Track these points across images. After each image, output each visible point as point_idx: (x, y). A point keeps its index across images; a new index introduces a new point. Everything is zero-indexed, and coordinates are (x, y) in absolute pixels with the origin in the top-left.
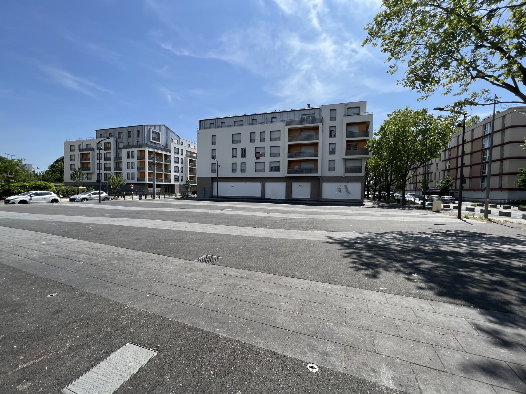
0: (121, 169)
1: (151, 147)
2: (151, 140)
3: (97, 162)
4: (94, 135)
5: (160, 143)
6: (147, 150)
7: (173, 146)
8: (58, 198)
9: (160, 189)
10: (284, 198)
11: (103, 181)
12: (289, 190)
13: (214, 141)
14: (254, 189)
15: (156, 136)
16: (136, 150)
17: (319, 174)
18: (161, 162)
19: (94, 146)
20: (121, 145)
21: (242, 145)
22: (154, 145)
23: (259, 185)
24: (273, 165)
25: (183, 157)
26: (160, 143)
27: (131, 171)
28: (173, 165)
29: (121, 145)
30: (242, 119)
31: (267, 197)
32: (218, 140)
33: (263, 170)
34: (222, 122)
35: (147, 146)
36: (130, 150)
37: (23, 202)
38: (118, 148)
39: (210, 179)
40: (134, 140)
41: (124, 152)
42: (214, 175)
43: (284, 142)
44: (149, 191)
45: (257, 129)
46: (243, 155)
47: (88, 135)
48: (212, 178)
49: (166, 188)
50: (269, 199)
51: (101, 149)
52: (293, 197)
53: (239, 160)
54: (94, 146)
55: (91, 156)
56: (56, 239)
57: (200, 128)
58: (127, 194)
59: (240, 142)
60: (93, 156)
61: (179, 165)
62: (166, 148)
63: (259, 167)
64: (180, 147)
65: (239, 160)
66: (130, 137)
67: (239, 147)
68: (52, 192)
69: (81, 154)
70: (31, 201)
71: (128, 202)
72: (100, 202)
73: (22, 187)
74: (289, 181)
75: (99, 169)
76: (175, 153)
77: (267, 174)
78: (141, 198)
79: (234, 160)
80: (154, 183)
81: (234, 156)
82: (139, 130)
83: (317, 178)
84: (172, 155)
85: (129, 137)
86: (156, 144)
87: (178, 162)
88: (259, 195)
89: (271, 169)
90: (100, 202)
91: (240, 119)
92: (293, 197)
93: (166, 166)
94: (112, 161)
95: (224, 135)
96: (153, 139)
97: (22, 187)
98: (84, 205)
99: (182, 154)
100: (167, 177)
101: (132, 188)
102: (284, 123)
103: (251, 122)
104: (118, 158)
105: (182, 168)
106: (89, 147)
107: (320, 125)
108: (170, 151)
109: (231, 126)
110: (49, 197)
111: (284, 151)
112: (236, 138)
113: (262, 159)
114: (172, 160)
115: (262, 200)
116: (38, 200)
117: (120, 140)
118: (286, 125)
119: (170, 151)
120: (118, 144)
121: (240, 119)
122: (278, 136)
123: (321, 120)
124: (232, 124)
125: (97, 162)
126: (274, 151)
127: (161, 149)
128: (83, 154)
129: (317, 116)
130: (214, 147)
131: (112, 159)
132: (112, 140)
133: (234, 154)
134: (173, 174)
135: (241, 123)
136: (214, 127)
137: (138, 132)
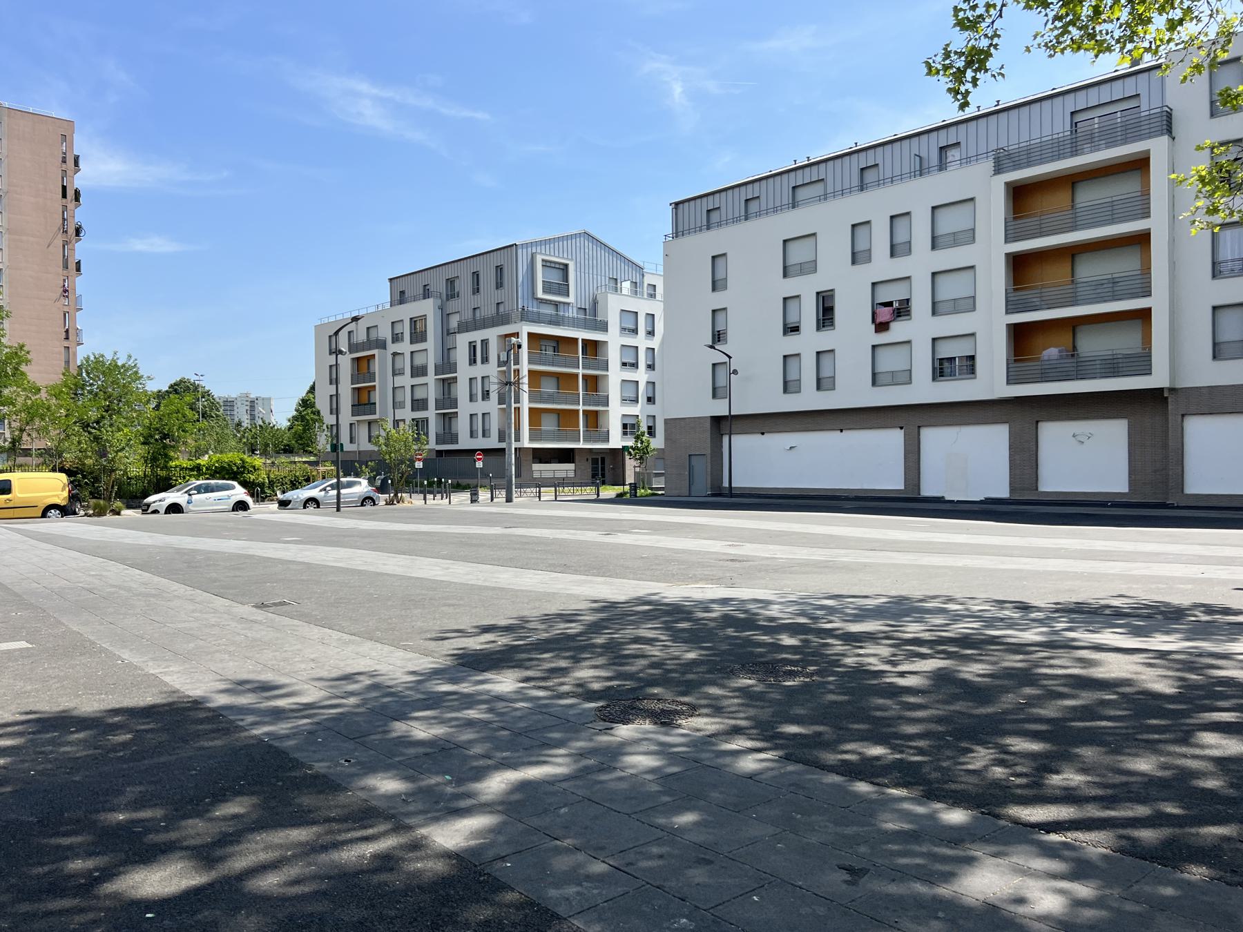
0: (454, 404)
1: (537, 319)
2: (540, 294)
3: (332, 390)
4: (384, 295)
5: (571, 299)
6: (526, 329)
7: (613, 307)
8: (249, 500)
9: (571, 466)
10: (1004, 493)
11: (348, 447)
12: (1024, 458)
13: (861, 246)
14: (874, 458)
15: (555, 277)
16: (492, 334)
17: (1158, 378)
18: (570, 364)
19: (385, 333)
20: (454, 322)
21: (819, 282)
22: (548, 310)
23: (892, 440)
24: (946, 351)
25: (655, 343)
26: (571, 299)
27: (480, 407)
28: (615, 377)
29: (454, 322)
30: (822, 171)
31: (929, 489)
32: (734, 271)
33: (905, 377)
34: (747, 199)
35: (525, 316)
36: (477, 336)
37: (175, 508)
38: (447, 333)
39: (708, 425)
40: (487, 302)
41: (462, 341)
42: (720, 408)
43: (990, 252)
44: (536, 475)
45: (875, 206)
46: (826, 314)
47: (369, 298)
48: (717, 421)
49: (595, 461)
50: (940, 500)
51: (341, 352)
52: (1042, 488)
53: (810, 340)
54: (385, 333)
55: (376, 366)
56: (88, 561)
57: (677, 234)
58: (458, 488)
59: (810, 267)
60: (381, 363)
61: (641, 375)
62: (592, 316)
63: (889, 361)
64: (643, 307)
65: (810, 340)
66: (466, 291)
67: (807, 288)
68: (235, 483)
69: (353, 359)
70: (191, 507)
71: (417, 510)
72: (338, 510)
73: (192, 470)
74: (1023, 415)
75: (335, 411)
76: (623, 329)
77: (924, 390)
78: (474, 500)
79: (791, 344)
80: (510, 444)
81: (791, 329)
82: (497, 266)
83: (1156, 396)
84: (614, 340)
85: (476, 290)
86: (556, 305)
87: (635, 365)
88: (894, 482)
89: (942, 369)
90: (338, 510)
91: (814, 174)
92: (1042, 488)
93: (594, 384)
94: (431, 378)
95: (753, 245)
96: (548, 288)
97: (192, 470)
98: (310, 518)
99: (651, 333)
100: (594, 420)
101: (479, 465)
102: (989, 165)
103: (856, 181)
104: (446, 365)
105: (651, 384)
106: (373, 336)
107: (1157, 148)
108: (604, 327)
109: (902, 177)
110: (229, 497)
111: (994, 280)
112: (799, 254)
113: (899, 331)
114: (614, 356)
115: (909, 502)
116: (202, 503)
117: (452, 305)
118: (998, 170)
119: (604, 327)
120: (445, 316)
121: (814, 174)
122: (808, 257)
123: (1166, 124)
124: (787, 198)
125: (332, 390)
126: (951, 289)
127: (575, 323)
128: (358, 359)
129: (1148, 105)
130: (718, 300)
131: (431, 369)
132: (427, 308)
133: (792, 319)
134: (616, 413)
135: (818, 189)
136: (879, 183)
137: (500, 269)
